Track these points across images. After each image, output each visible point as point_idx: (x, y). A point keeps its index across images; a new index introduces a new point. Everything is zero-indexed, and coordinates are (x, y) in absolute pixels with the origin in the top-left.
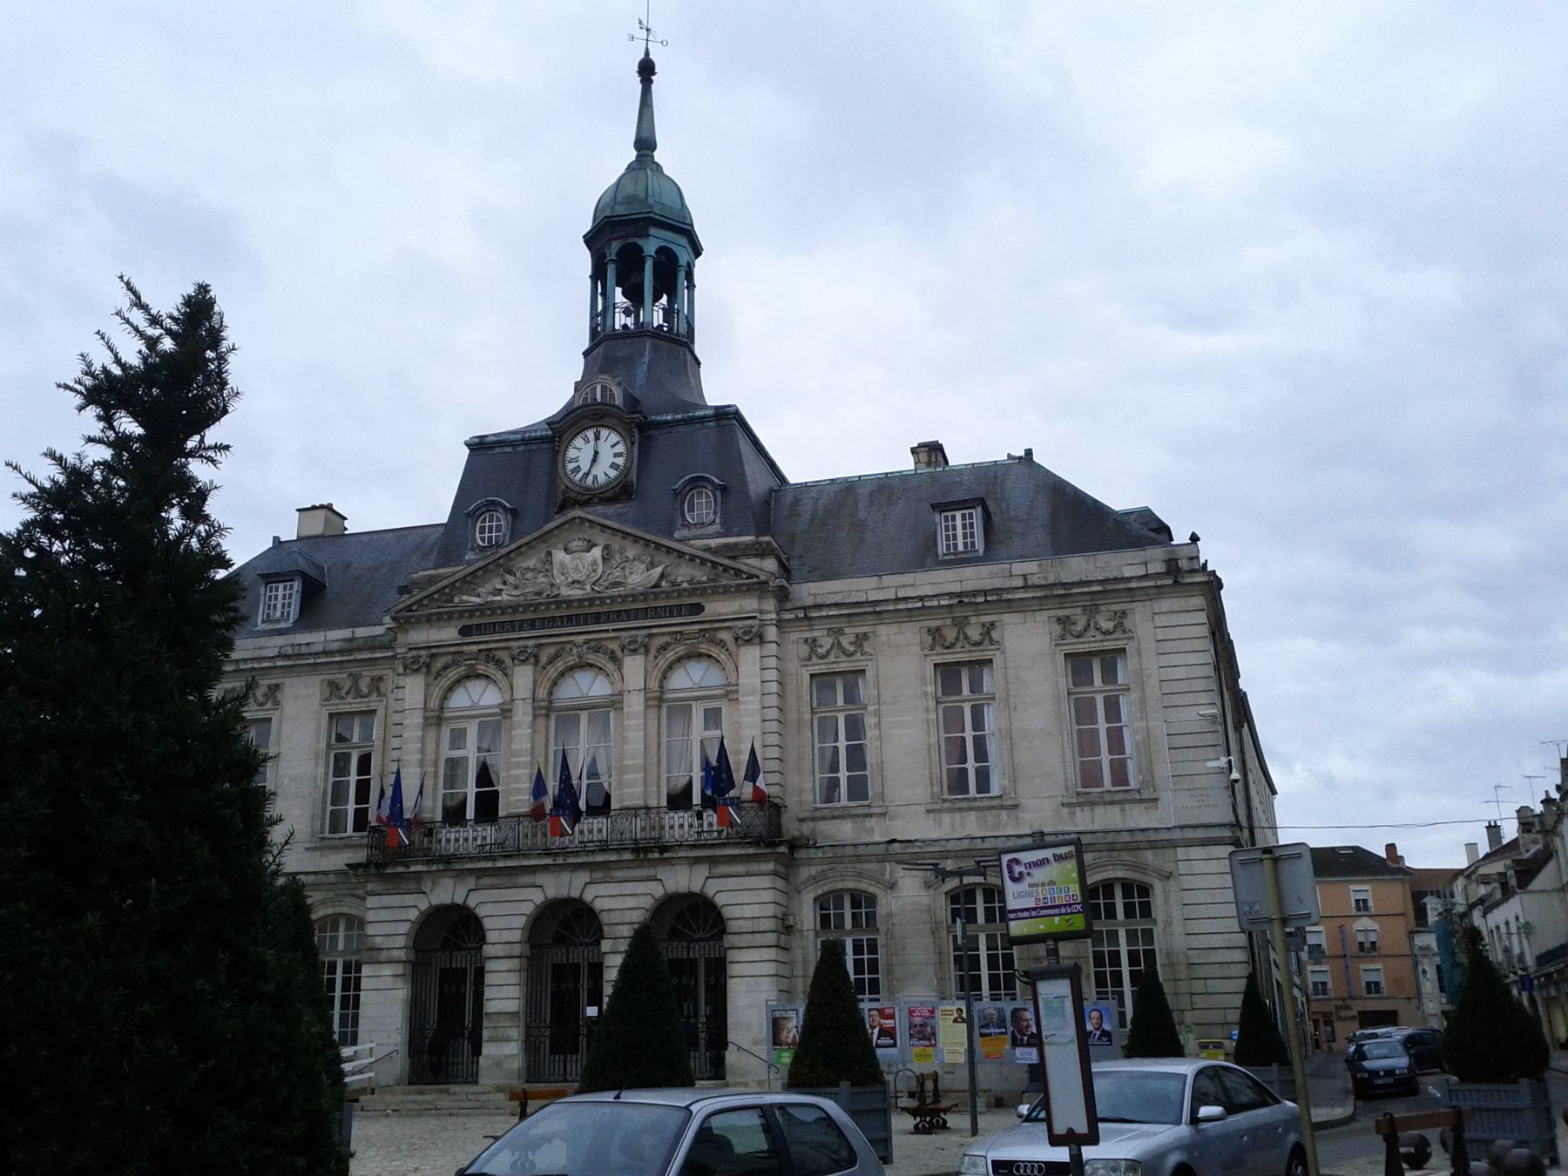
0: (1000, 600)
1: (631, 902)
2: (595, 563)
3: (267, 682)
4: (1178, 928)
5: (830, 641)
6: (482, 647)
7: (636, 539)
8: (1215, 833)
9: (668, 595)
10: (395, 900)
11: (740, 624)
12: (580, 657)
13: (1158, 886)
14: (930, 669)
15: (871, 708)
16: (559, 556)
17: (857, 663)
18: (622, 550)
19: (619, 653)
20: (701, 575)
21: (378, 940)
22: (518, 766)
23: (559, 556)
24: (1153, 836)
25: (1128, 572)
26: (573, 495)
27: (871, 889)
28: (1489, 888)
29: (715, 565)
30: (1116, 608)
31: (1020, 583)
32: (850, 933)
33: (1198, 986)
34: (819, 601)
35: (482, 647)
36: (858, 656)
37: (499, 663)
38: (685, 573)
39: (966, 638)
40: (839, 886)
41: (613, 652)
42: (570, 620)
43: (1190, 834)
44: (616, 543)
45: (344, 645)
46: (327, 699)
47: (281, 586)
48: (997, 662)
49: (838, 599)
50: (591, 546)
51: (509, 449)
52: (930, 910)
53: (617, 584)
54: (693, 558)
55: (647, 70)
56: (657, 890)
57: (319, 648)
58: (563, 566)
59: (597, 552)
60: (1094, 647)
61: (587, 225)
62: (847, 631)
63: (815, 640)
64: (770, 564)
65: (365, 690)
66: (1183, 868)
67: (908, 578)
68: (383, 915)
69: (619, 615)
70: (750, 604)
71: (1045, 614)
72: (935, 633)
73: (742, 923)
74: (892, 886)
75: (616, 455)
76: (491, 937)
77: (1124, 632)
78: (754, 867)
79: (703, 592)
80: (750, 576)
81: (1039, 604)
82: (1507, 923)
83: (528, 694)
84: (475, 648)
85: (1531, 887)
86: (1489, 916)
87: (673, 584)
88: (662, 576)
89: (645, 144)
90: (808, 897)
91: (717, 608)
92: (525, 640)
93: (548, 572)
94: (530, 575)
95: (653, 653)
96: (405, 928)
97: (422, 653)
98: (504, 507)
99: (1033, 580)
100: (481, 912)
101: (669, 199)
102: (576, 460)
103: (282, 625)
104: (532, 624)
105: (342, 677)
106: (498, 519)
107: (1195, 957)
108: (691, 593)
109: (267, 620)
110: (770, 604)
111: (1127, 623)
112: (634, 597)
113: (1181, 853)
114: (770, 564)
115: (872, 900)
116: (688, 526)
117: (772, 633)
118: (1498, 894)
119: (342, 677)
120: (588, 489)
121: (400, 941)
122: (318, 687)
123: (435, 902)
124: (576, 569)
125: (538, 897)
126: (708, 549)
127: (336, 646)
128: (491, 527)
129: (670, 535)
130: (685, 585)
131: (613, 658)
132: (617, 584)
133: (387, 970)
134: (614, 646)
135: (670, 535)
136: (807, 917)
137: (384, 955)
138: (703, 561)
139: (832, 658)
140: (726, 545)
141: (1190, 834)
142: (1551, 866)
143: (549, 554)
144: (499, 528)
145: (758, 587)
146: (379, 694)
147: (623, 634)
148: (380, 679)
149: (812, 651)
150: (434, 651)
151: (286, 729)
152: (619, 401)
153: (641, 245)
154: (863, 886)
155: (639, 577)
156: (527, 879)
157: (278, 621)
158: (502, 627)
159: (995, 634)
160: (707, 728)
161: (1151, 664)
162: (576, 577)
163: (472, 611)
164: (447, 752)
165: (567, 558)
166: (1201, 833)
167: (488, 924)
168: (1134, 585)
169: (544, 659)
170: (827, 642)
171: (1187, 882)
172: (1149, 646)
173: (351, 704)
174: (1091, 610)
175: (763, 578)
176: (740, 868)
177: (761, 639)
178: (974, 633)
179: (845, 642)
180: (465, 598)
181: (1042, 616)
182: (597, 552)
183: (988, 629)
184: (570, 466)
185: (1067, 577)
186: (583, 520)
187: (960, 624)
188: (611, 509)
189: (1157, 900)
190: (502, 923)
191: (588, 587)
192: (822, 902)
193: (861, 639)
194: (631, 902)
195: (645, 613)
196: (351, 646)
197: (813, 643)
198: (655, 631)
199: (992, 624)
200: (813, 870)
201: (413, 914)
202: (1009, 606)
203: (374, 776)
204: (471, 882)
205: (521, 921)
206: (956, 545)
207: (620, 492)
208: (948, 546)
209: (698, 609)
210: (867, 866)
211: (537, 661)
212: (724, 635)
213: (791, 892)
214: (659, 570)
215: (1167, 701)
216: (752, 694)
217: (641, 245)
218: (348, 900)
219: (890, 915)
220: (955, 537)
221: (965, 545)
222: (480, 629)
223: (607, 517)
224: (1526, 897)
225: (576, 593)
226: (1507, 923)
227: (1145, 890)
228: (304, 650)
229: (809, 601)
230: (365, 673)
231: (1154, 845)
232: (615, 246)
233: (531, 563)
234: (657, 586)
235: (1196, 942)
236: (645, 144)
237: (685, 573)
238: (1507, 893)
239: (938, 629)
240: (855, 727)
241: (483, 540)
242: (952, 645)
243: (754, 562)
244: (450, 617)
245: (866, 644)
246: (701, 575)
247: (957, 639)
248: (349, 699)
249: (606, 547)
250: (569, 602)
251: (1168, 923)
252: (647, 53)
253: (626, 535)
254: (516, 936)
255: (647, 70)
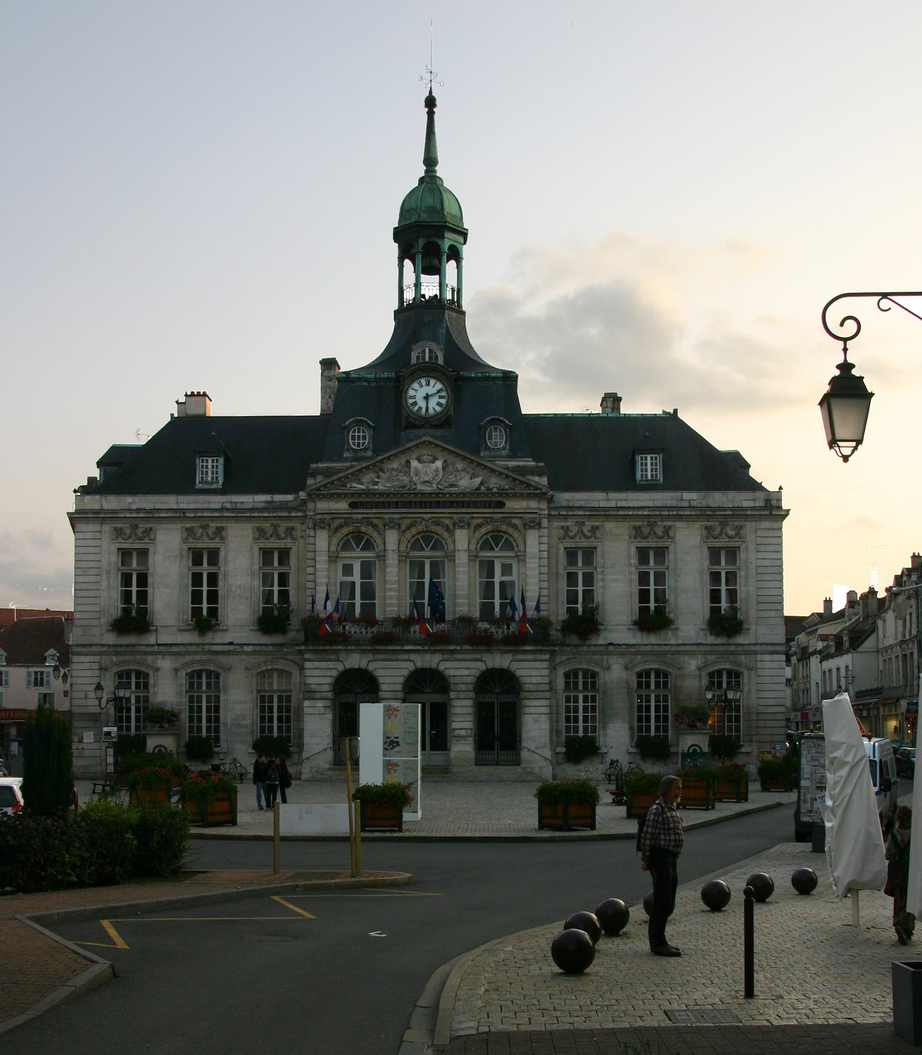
0: (678, 514)
1: (466, 672)
2: (437, 470)
3: (214, 525)
4: (753, 695)
5: (577, 528)
6: (365, 516)
7: (465, 458)
8: (777, 648)
9: (486, 495)
10: (323, 664)
11: (528, 516)
12: (427, 527)
13: (746, 673)
14: (633, 551)
15: (599, 570)
16: (415, 464)
17: (592, 543)
18: (453, 464)
19: (451, 527)
20: (504, 484)
21: (313, 686)
22: (391, 590)
23: (415, 464)
24: (747, 648)
25: (745, 504)
26: (412, 420)
27: (596, 669)
28: (825, 643)
29: (514, 479)
30: (737, 523)
31: (687, 504)
32: (581, 692)
33: (761, 723)
34: (571, 504)
35: (365, 516)
36: (592, 539)
37: (375, 527)
38: (495, 482)
39: (655, 534)
40: (578, 667)
41: (447, 526)
42: (421, 505)
43: (765, 648)
44: (451, 459)
45: (266, 505)
46: (258, 539)
47: (210, 460)
48: (671, 549)
49: (582, 504)
50: (435, 459)
51: (366, 384)
52: (627, 682)
53: (452, 485)
54: (500, 474)
55: (430, 103)
56: (482, 666)
57: (250, 506)
58: (417, 471)
59: (439, 464)
60: (724, 545)
61: (394, 221)
62: (587, 523)
63: (568, 527)
64: (544, 481)
65: (283, 535)
66: (759, 665)
67: (623, 495)
68: (316, 673)
69: (452, 504)
70: (533, 504)
71: (699, 523)
72: (637, 529)
73: (531, 686)
74: (608, 668)
75: (421, 386)
76: (384, 687)
77: (740, 537)
78: (539, 657)
79: (507, 495)
80: (536, 489)
81: (696, 518)
82: (838, 669)
83: (396, 547)
84: (360, 516)
85: (859, 650)
86: (824, 663)
87: (488, 489)
88: (482, 483)
89: (430, 161)
90: (561, 672)
91: (513, 505)
92: (391, 514)
93: (407, 473)
94: (394, 473)
95: (472, 528)
96: (330, 680)
97: (326, 516)
98: (369, 425)
99: (694, 504)
100: (377, 673)
101: (454, 210)
102: (414, 397)
103: (214, 486)
104: (396, 505)
105: (266, 525)
106: (364, 432)
107: (761, 709)
108: (500, 495)
109: (202, 481)
110: (544, 505)
111: (742, 533)
112: (464, 494)
113: (759, 657)
114: (544, 481)
115: (594, 675)
116: (489, 449)
117: (545, 522)
118: (833, 650)
119: (266, 525)
120: (422, 417)
121: (326, 688)
122: (250, 531)
123: (348, 667)
124: (426, 473)
125: (411, 667)
126: (507, 468)
127: (261, 505)
128: (359, 436)
129: (478, 455)
130: (495, 490)
131: (448, 530)
132: (452, 485)
133: (320, 704)
134: (447, 522)
135: (478, 455)
136: (560, 683)
137: (318, 695)
138: (507, 477)
139: (577, 539)
140: (518, 466)
141: (765, 648)
142: (873, 636)
143: (408, 462)
144: (364, 438)
145: (540, 495)
146: (292, 538)
147: (454, 516)
148: (293, 529)
149: (566, 534)
150: (334, 515)
151: (231, 556)
152: (441, 361)
153: (428, 232)
154: (591, 668)
155: (466, 483)
156: (405, 656)
157: (211, 483)
158: (377, 505)
159: (671, 533)
160: (502, 575)
161: (752, 557)
162: (427, 479)
163: (360, 494)
164: (341, 578)
165: (420, 466)
166: (770, 648)
167: (381, 680)
168: (749, 513)
169: (403, 527)
170: (575, 529)
171: (760, 672)
172: (752, 546)
173: (273, 543)
174: (724, 524)
175: (544, 490)
176: (530, 657)
177: (539, 526)
178: (660, 532)
179: (585, 530)
180: (354, 485)
181: (698, 525)
182: (439, 464)
183: (667, 530)
184: (411, 401)
185: (713, 504)
186: (430, 443)
187: (652, 525)
188: (439, 432)
189: (745, 679)
190: (390, 680)
191: (435, 486)
192: (567, 675)
193: (594, 529)
194: (466, 672)
195: (469, 504)
196: (271, 507)
197: (566, 529)
198: (474, 515)
199: (670, 527)
200: (564, 658)
201: (335, 673)
202: (680, 518)
203: (292, 589)
204: (370, 657)
205: (401, 680)
206: (646, 475)
207: (442, 422)
208: (642, 475)
209: (501, 505)
210: (594, 657)
211: (399, 527)
212: (516, 521)
213: (553, 668)
214: (479, 480)
215: (759, 577)
216: (534, 558)
217: (428, 232)
218: (282, 661)
219: (605, 683)
220: (646, 471)
221: (652, 475)
222: (363, 505)
223: (436, 438)
224: (855, 655)
225: (428, 489)
226: (838, 669)
227: (738, 675)
228: (239, 506)
229: (565, 504)
230: (282, 524)
231: (745, 653)
232: (421, 242)
233: (395, 465)
234: (478, 489)
235: (762, 702)
236: (430, 161)
237: (495, 482)
238: (840, 650)
239: (640, 527)
240: (589, 579)
241: (354, 444)
242: (647, 537)
243: (536, 479)
244: (346, 495)
245: (597, 532)
246: (504, 484)
247: (650, 533)
248: (272, 540)
249: (445, 462)
250: (423, 494)
251: (749, 692)
252: (431, 92)
253: (458, 455)
254: (399, 687)
255: (430, 103)
